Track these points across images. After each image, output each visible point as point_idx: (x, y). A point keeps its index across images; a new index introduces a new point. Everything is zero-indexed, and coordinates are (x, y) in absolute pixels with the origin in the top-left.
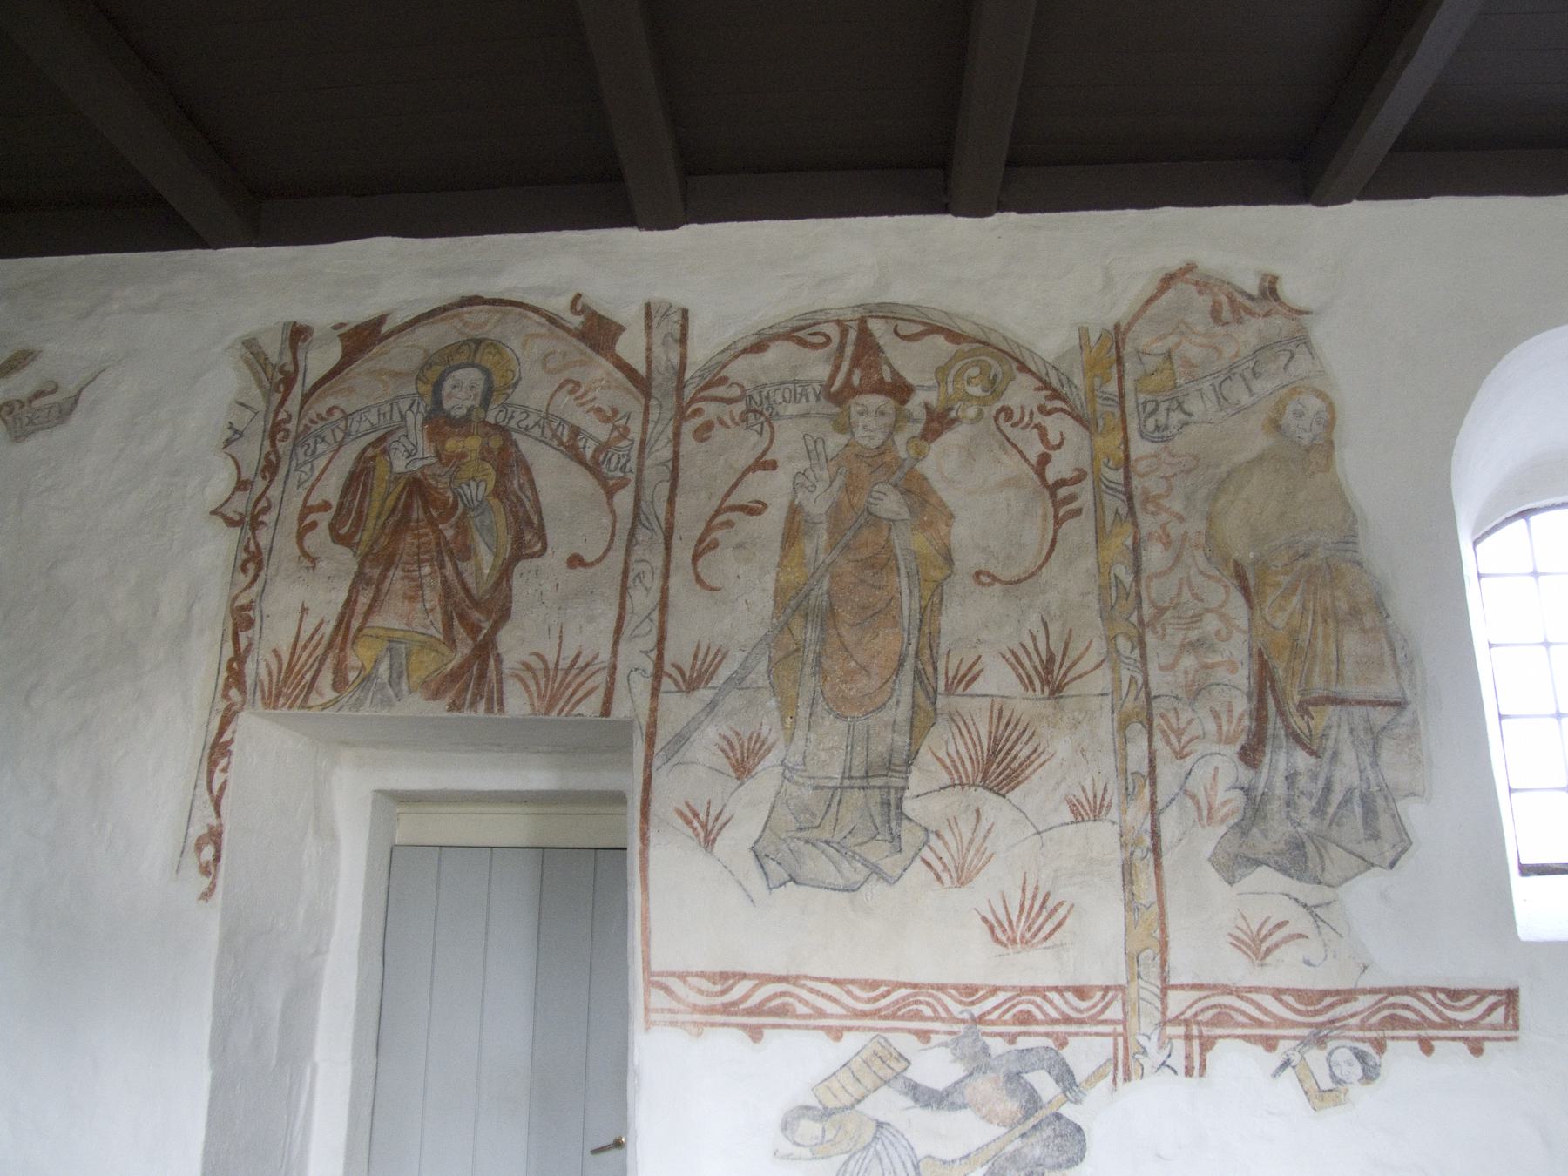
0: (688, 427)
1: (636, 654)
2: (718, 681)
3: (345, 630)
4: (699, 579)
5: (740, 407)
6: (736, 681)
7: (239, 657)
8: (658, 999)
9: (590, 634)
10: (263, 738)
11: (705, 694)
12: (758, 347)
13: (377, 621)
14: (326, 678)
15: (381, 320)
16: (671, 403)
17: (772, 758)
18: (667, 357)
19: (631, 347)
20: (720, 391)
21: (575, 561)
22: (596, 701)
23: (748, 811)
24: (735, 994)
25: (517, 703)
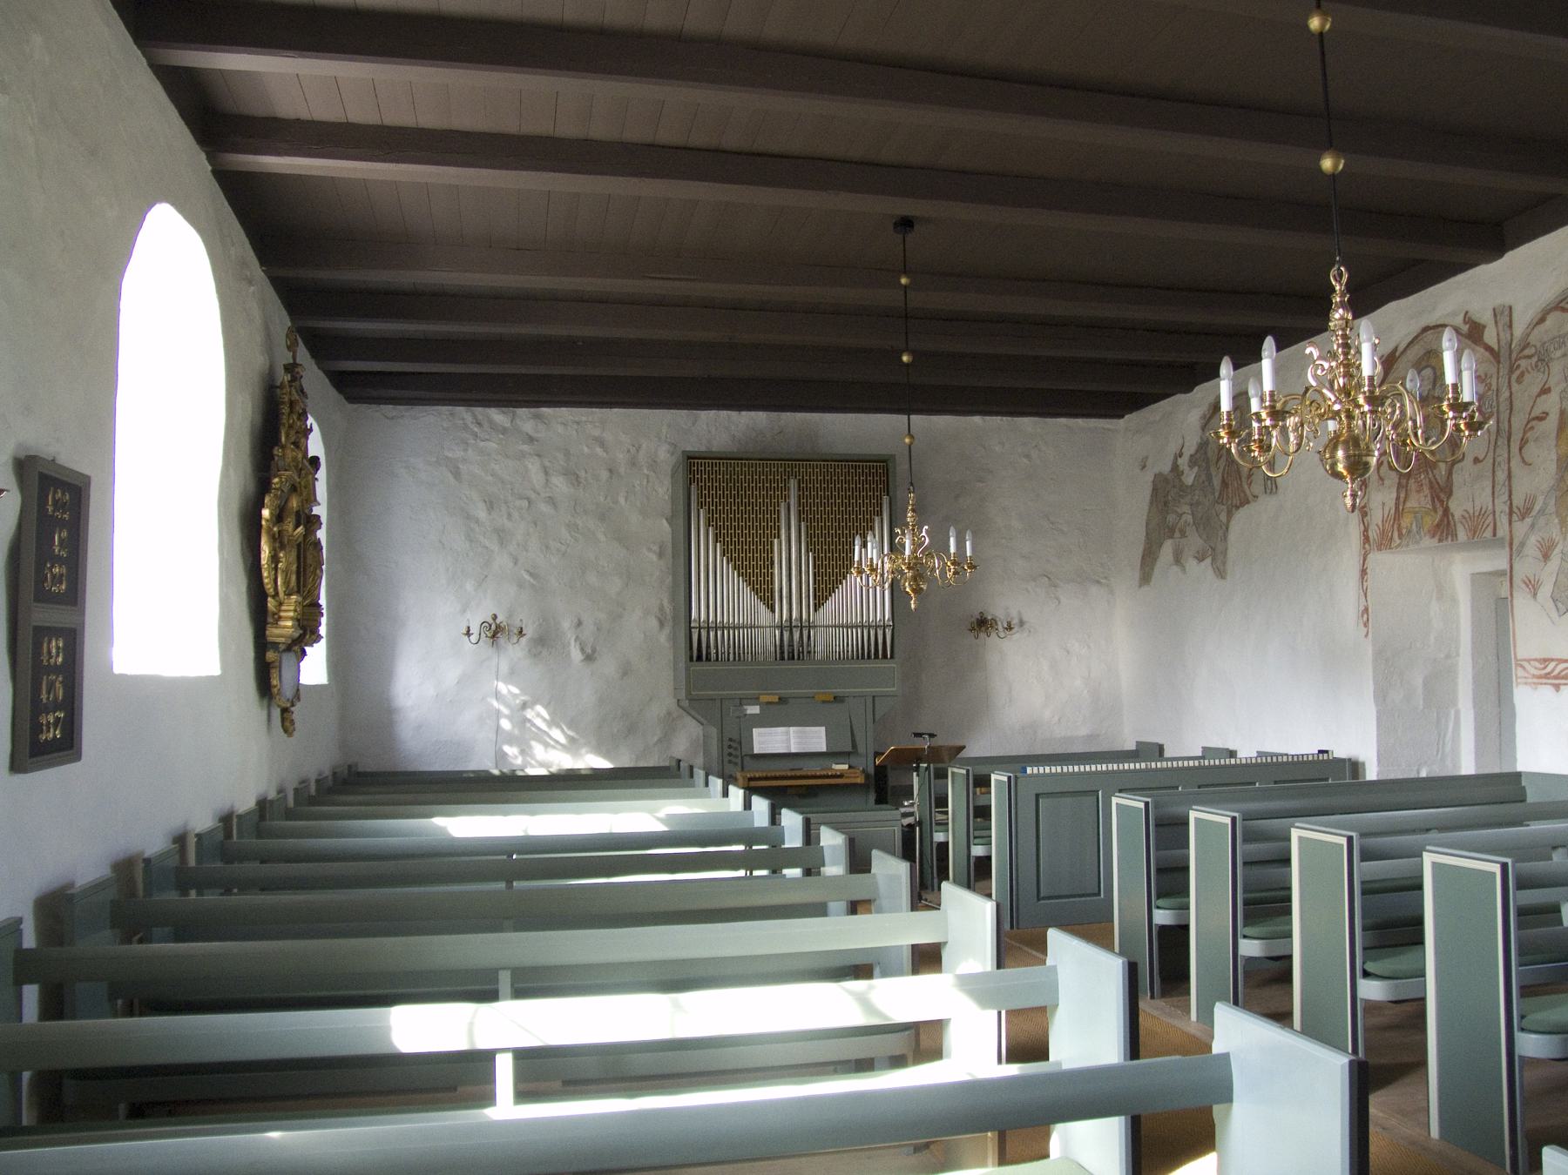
0: (1514, 377)
1: (1501, 506)
2: (1534, 513)
3: (1399, 513)
4: (1524, 461)
5: (1535, 359)
6: (1542, 512)
7: (1366, 530)
8: (1520, 672)
9: (1483, 498)
10: (1381, 561)
11: (1528, 520)
12: (1542, 320)
13: (1408, 505)
14: (1396, 534)
15: (1396, 349)
16: (1507, 365)
17: (1557, 551)
18: (1505, 336)
19: (1490, 337)
20: (1527, 352)
21: (1476, 461)
22: (1490, 529)
23: (1548, 575)
24: (1549, 669)
25: (1462, 535)
